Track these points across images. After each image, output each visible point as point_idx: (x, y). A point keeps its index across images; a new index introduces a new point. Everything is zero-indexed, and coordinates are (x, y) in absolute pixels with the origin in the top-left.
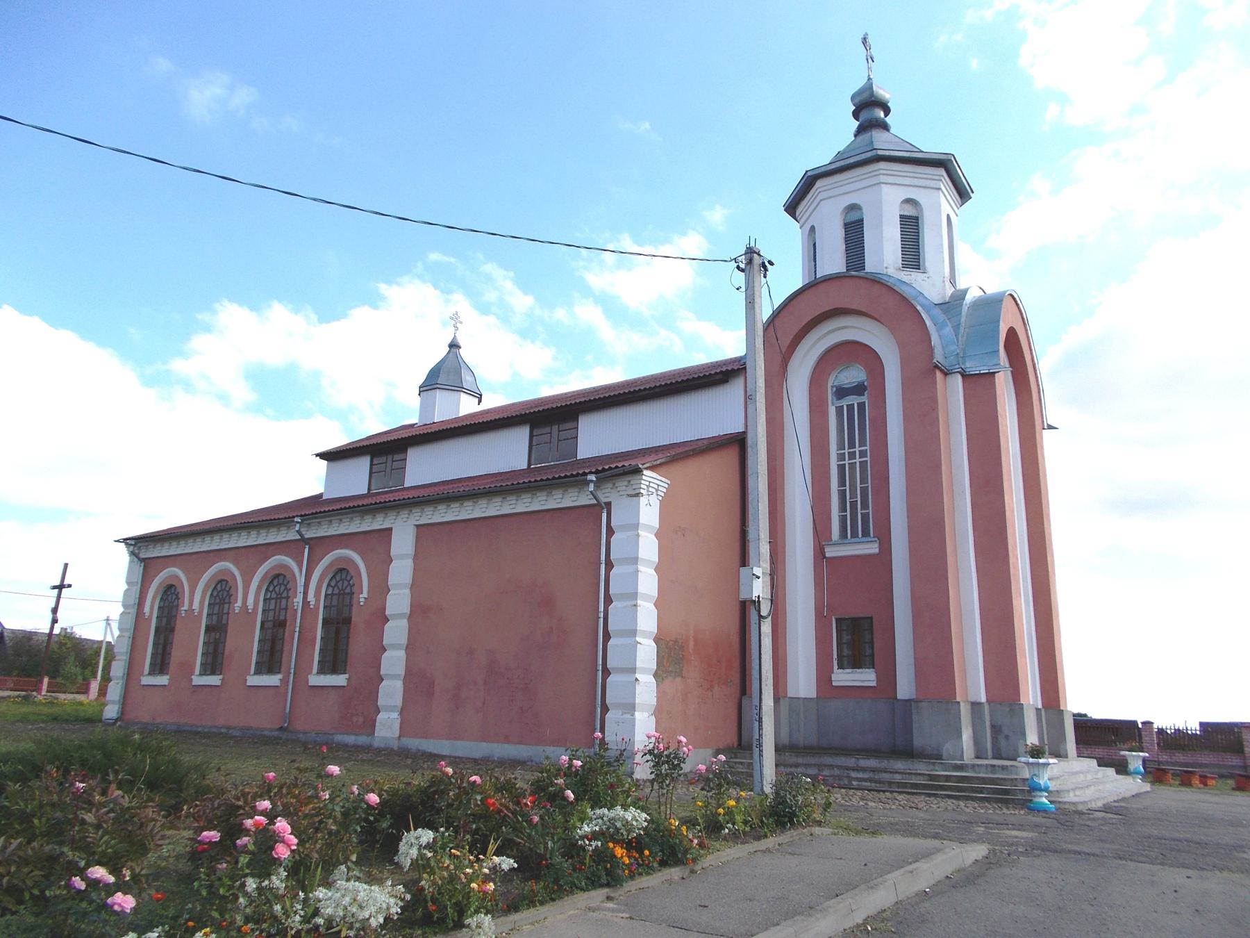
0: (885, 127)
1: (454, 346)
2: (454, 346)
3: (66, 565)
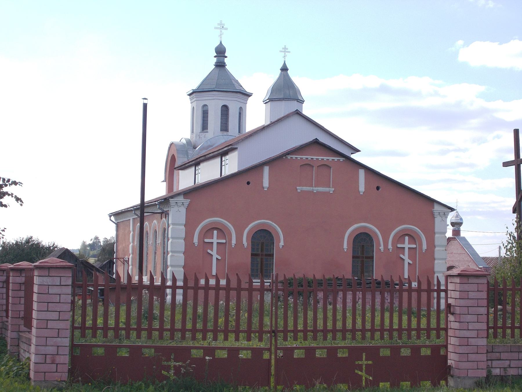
1: (284, 69)
2: (284, 69)
3: (145, 106)
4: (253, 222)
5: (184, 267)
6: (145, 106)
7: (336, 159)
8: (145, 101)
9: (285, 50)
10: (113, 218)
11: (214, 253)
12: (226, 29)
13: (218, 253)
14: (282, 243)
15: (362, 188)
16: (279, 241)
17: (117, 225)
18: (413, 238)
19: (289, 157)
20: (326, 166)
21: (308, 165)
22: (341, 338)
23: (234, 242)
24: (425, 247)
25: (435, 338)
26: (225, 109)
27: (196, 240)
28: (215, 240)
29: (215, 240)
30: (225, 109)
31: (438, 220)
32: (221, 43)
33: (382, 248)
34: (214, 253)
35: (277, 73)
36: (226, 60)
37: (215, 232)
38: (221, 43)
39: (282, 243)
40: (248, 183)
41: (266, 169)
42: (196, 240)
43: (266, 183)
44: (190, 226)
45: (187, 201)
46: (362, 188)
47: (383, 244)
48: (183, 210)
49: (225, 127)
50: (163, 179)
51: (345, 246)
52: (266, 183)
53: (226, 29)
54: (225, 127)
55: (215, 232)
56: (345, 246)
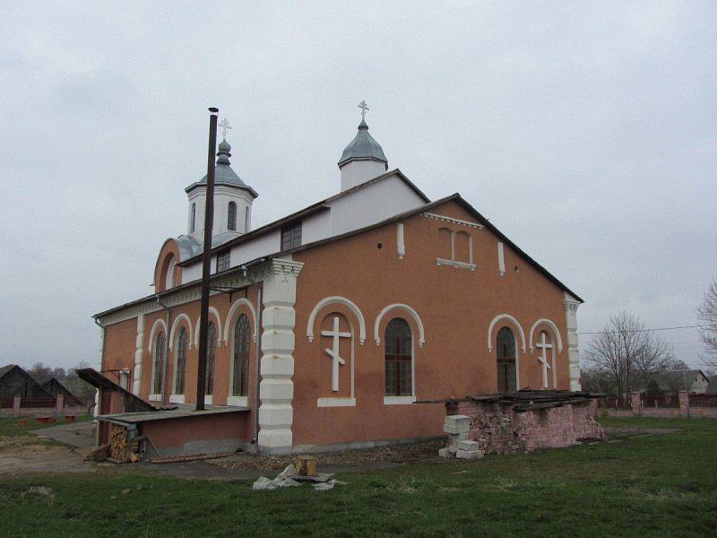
0: (228, 164)
1: (363, 127)
2: (363, 127)
3: (214, 120)
4: (391, 304)
5: (293, 378)
6: (214, 120)
7: (476, 225)
8: (215, 114)
9: (363, 106)
10: (98, 321)
11: (335, 352)
12: (230, 128)
13: (340, 355)
14: (422, 340)
15: (502, 267)
16: (418, 337)
17: (106, 329)
18: (345, 325)
19: (426, 215)
20: (464, 233)
21: (446, 230)
22: (9, 410)
23: (363, 336)
24: (560, 347)
25: (54, 410)
26: (232, 205)
27: (310, 332)
28: (336, 333)
29: (336, 333)
30: (232, 205)
31: (569, 313)
32: (363, 120)
33: (524, 347)
34: (335, 352)
35: (353, 133)
36: (229, 159)
37: (337, 320)
38: (363, 120)
39: (422, 340)
40: (380, 246)
41: (401, 228)
42: (310, 332)
43: (401, 249)
44: (302, 307)
45: (299, 265)
46: (502, 267)
47: (523, 343)
48: (292, 280)
49: (232, 226)
50: (152, 282)
51: (490, 346)
52: (401, 249)
53: (230, 128)
54: (232, 226)
55: (337, 320)
56: (490, 346)
